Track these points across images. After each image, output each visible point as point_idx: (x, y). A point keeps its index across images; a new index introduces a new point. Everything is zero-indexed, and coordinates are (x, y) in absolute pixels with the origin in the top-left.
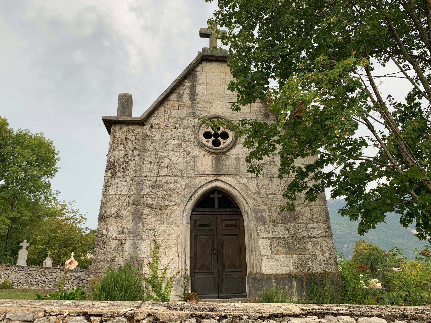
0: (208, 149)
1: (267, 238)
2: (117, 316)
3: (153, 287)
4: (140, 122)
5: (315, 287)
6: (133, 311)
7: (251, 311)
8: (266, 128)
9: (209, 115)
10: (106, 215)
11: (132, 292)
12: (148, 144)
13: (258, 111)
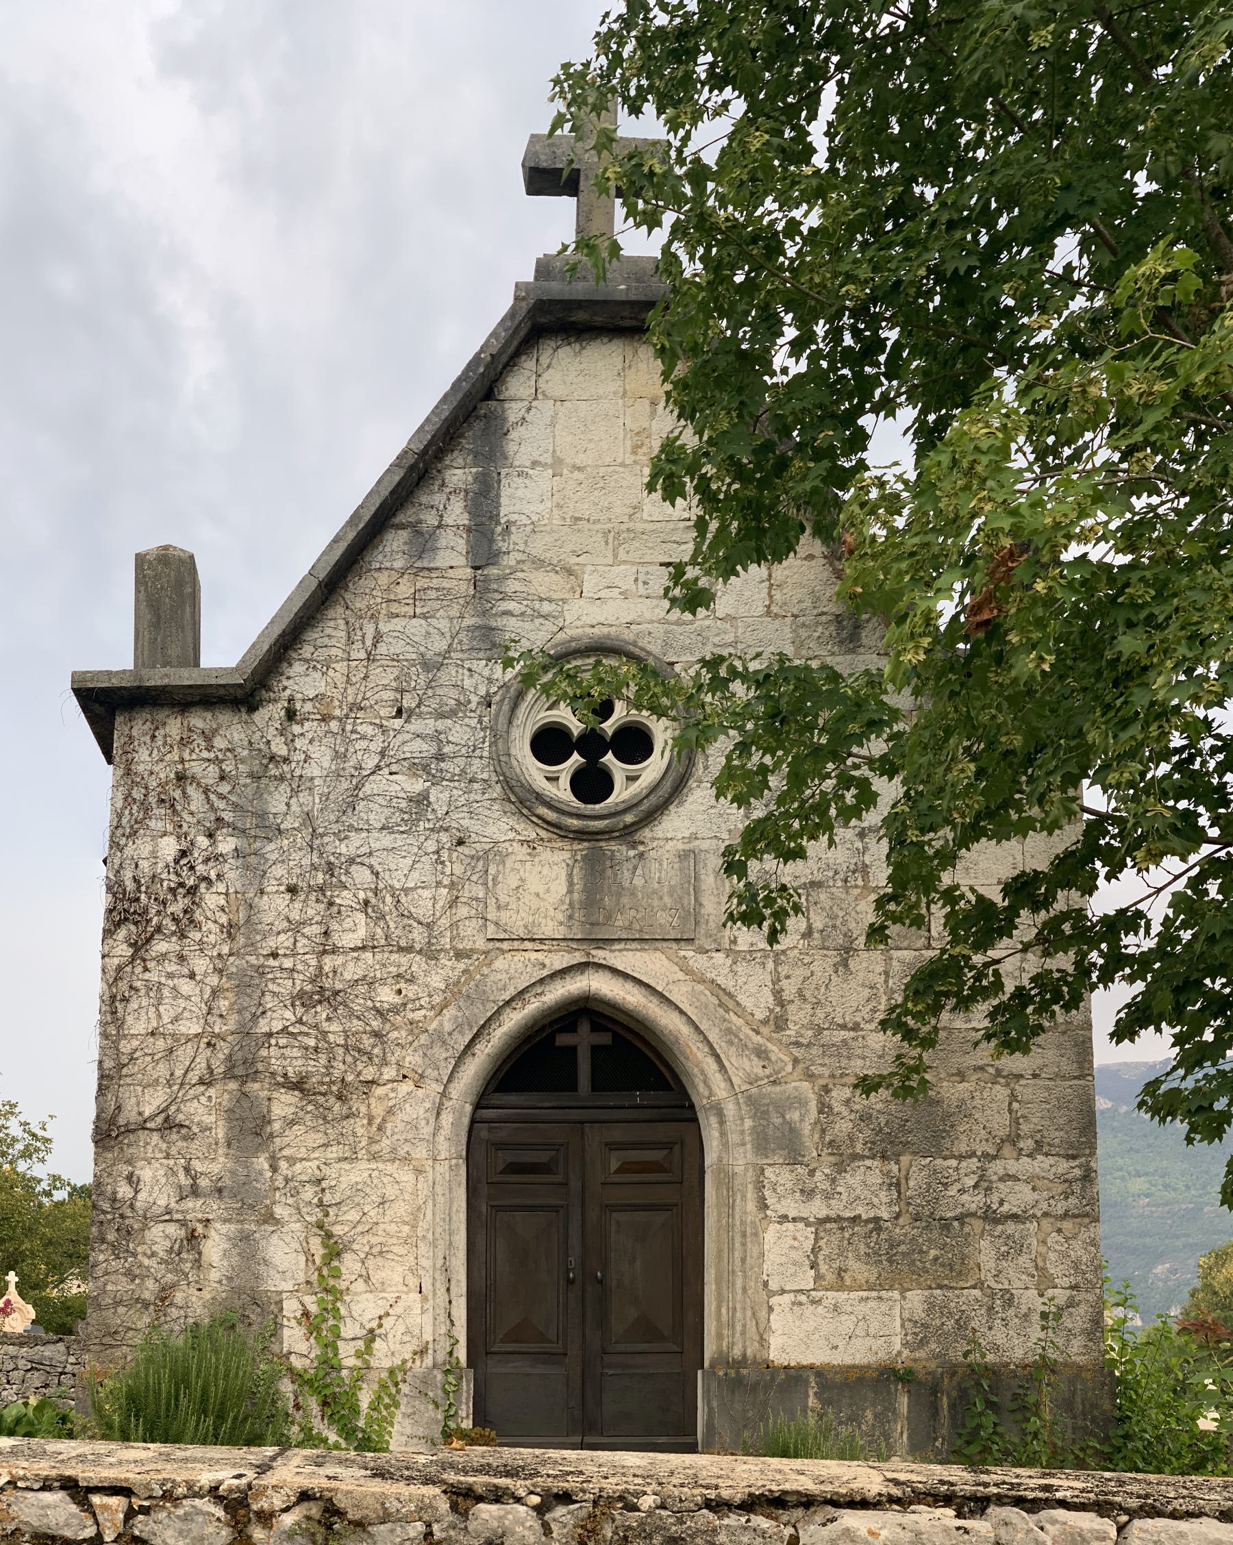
0: (551, 815)
1: (802, 1219)
2: (185, 1497)
3: (325, 1404)
4: (239, 693)
5: (990, 1419)
6: (244, 1481)
7: (675, 1481)
8: (834, 697)
9: (561, 636)
10: (121, 1121)
11: (245, 1419)
12: (277, 802)
13: (808, 604)
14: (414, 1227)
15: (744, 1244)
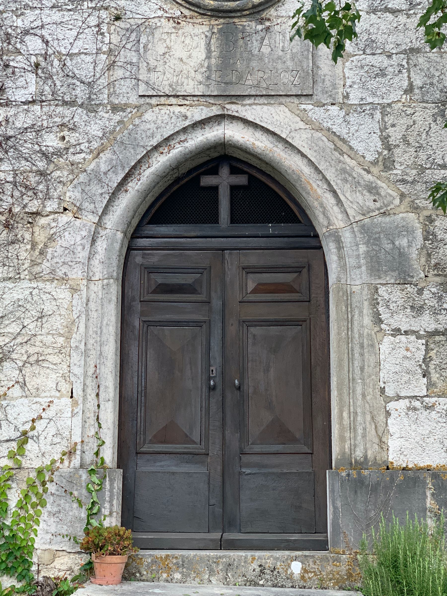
14: (68, 339)
15: (362, 355)
